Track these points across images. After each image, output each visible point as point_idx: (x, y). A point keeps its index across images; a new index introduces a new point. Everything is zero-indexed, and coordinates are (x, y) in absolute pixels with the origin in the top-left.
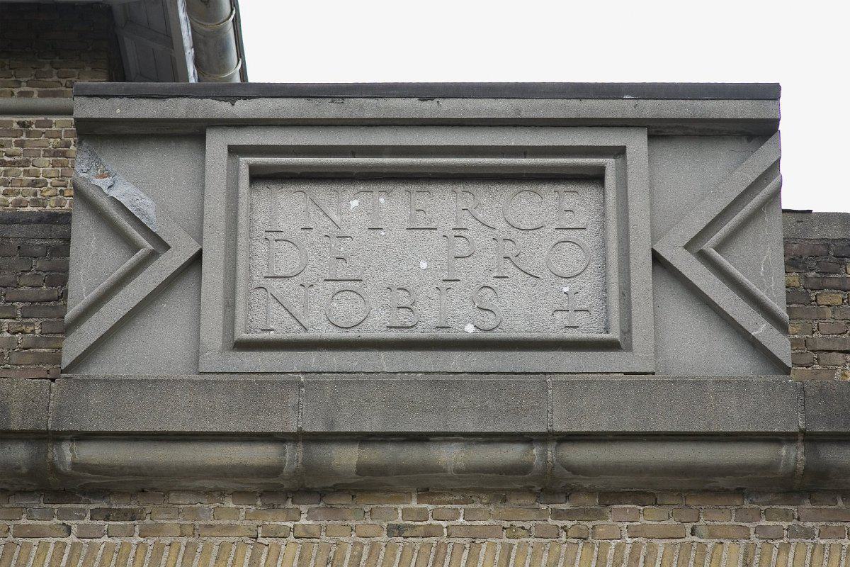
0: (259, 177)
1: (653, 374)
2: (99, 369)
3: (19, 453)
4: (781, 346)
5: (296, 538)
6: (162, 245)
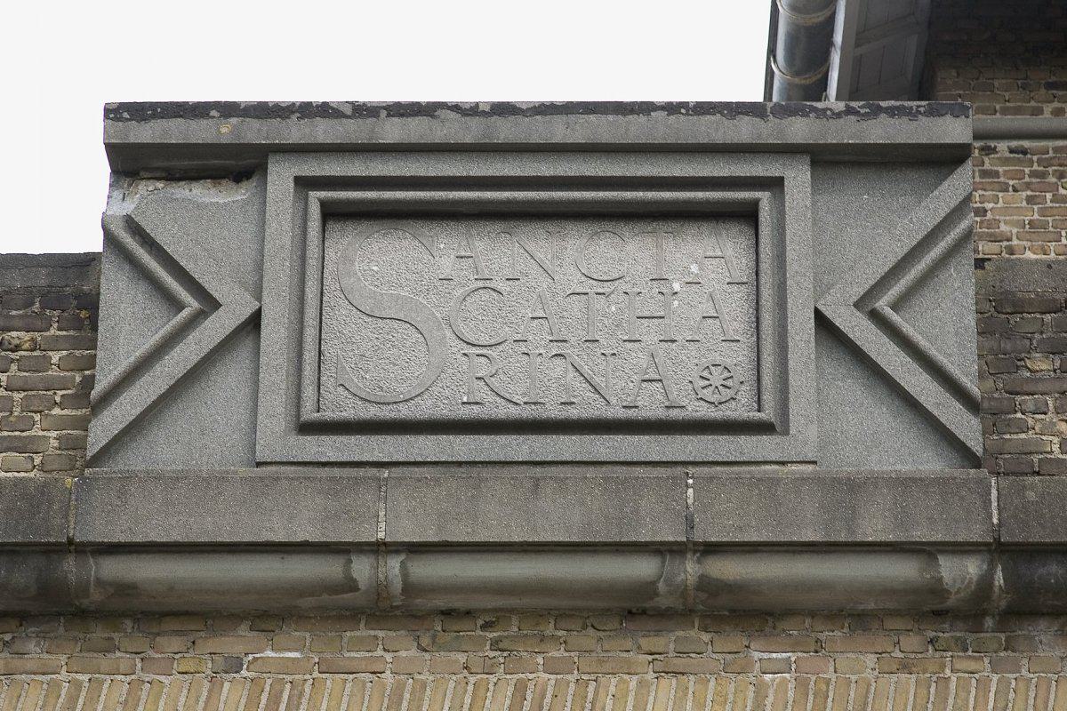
0: (332, 213)
1: (814, 463)
2: (134, 459)
3: (23, 576)
4: (968, 428)
5: (320, 673)
6: (210, 304)
